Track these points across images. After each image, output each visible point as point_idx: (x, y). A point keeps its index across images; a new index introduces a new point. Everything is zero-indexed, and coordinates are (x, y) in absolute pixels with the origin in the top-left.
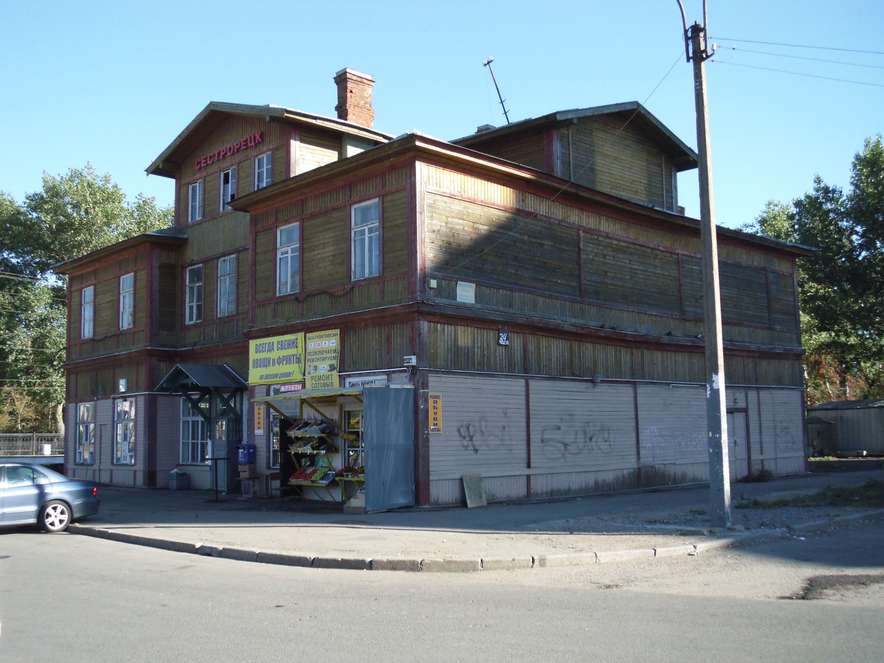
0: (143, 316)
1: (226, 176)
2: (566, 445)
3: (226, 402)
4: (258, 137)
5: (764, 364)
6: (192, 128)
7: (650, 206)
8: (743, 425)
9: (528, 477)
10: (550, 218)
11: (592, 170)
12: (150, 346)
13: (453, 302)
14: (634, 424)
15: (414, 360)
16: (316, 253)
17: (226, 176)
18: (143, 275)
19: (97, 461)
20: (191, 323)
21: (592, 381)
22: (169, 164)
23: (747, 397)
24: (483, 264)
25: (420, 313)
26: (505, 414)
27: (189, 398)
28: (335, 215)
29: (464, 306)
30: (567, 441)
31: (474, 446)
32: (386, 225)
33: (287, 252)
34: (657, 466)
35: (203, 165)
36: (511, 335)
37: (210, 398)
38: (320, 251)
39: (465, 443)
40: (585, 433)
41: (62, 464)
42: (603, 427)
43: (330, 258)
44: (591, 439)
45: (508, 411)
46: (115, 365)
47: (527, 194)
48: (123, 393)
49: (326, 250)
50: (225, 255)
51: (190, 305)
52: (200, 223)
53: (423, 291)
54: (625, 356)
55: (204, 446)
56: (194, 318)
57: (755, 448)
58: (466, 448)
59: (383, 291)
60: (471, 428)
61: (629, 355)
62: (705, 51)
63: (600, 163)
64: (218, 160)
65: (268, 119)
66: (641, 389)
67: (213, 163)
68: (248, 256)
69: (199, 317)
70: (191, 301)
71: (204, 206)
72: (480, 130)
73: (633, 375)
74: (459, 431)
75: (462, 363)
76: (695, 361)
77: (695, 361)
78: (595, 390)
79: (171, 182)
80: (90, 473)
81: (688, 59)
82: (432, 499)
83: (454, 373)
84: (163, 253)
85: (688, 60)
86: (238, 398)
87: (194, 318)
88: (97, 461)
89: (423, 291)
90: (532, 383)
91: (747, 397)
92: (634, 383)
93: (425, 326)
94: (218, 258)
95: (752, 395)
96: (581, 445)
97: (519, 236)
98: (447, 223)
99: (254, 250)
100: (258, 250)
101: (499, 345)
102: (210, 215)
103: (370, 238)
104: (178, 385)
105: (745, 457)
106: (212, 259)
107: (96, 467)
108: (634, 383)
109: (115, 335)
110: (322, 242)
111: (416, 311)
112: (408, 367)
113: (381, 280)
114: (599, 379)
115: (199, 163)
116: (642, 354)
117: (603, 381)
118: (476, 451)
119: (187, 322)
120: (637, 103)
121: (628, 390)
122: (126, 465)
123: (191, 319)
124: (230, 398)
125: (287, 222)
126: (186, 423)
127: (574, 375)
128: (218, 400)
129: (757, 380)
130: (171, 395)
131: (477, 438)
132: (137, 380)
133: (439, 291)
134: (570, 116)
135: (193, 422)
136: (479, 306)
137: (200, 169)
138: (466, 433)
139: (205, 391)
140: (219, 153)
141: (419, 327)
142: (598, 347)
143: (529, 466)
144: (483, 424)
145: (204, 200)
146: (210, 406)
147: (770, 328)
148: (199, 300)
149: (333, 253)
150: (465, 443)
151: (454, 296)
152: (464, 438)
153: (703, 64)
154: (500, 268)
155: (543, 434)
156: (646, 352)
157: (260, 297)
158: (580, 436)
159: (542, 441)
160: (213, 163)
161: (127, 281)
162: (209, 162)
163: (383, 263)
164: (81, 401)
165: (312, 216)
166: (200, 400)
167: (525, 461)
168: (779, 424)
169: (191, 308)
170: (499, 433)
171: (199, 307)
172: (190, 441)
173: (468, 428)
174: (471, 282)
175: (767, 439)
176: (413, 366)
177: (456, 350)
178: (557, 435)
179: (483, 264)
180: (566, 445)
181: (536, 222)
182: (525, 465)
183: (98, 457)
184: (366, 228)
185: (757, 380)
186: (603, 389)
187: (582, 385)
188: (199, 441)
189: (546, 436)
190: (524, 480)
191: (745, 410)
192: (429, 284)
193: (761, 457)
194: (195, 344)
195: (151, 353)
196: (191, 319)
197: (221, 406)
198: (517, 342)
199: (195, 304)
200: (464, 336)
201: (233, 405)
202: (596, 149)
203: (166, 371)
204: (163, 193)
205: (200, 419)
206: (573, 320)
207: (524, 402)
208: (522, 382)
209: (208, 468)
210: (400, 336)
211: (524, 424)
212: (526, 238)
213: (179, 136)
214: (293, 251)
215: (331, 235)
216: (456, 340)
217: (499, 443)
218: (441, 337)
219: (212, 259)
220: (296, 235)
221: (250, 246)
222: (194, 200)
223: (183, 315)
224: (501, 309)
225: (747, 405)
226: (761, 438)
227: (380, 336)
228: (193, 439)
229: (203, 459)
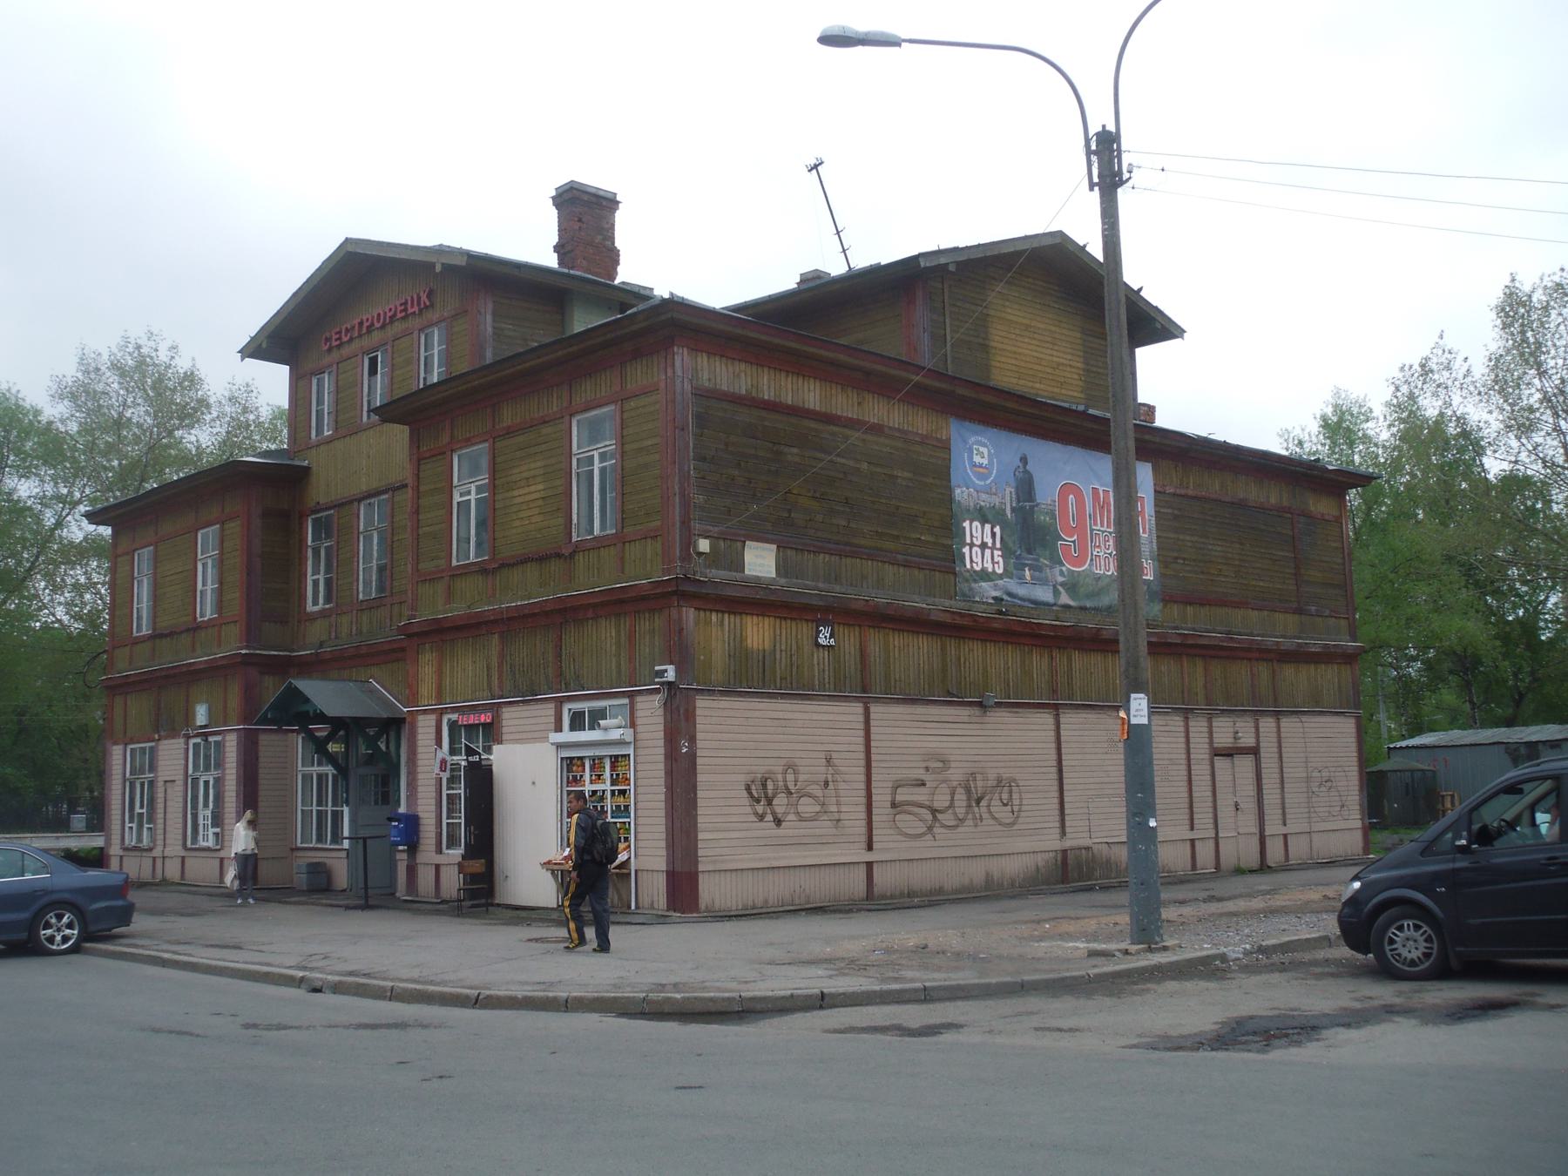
0: (235, 596)
1: (373, 362)
2: (934, 811)
3: (372, 742)
4: (424, 297)
5: (1288, 671)
6: (302, 295)
7: (1081, 408)
8: (1252, 775)
9: (869, 865)
10: (905, 432)
11: (985, 348)
12: (247, 647)
13: (738, 575)
14: (1055, 776)
15: (671, 674)
16: (516, 493)
17: (373, 362)
18: (235, 527)
19: (160, 842)
20: (316, 608)
21: (980, 704)
22: (281, 340)
23: (1279, 727)
24: (789, 511)
25: (685, 597)
26: (829, 760)
27: (310, 735)
28: (546, 430)
29: (758, 584)
30: (936, 805)
31: (774, 814)
32: (628, 447)
33: (469, 493)
34: (1095, 847)
35: (345, 339)
36: (840, 630)
37: (347, 734)
38: (522, 491)
39: (760, 809)
40: (968, 791)
41: (102, 849)
42: (999, 780)
43: (540, 502)
44: (978, 801)
45: (834, 755)
46: (190, 678)
47: (866, 394)
48: (202, 727)
49: (533, 488)
50: (370, 495)
51: (314, 578)
52: (329, 441)
53: (686, 557)
54: (1039, 663)
55: (337, 817)
56: (321, 601)
57: (1272, 815)
58: (761, 818)
59: (622, 559)
60: (770, 785)
61: (1046, 660)
62: (1120, 173)
63: (998, 336)
64: (360, 336)
65: (438, 268)
66: (1068, 718)
67: (351, 339)
68: (406, 497)
69: (328, 599)
70: (316, 571)
71: (337, 413)
72: (804, 279)
73: (1054, 692)
74: (748, 789)
75: (753, 678)
76: (1164, 668)
77: (1164, 668)
78: (987, 719)
79: (284, 370)
80: (147, 863)
81: (1092, 186)
82: (702, 906)
83: (741, 694)
84: (265, 495)
85: (1091, 189)
86: (392, 734)
87: (321, 601)
88: (160, 842)
89: (686, 557)
90: (874, 708)
91: (1279, 727)
92: (1056, 707)
93: (690, 615)
94: (359, 500)
95: (1267, 724)
96: (961, 811)
97: (851, 463)
98: (727, 445)
99: (417, 489)
100: (422, 488)
101: (818, 645)
102: (346, 428)
103: (603, 471)
104: (293, 713)
105: (1255, 830)
106: (351, 502)
107: (157, 852)
108: (1056, 707)
109: (188, 630)
110: (525, 475)
111: (675, 593)
112: (662, 684)
113: (619, 540)
114: (992, 702)
115: (327, 340)
116: (1070, 660)
117: (999, 705)
118: (778, 822)
119: (310, 608)
120: (1061, 232)
121: (1047, 719)
122: (208, 849)
123: (315, 603)
124: (378, 737)
125: (469, 442)
126: (307, 778)
127: (950, 694)
128: (360, 740)
129: (1276, 700)
130: (279, 731)
131: (780, 802)
132: (225, 707)
133: (713, 559)
134: (943, 261)
135: (320, 776)
136: (783, 581)
137: (330, 350)
138: (761, 793)
139: (338, 724)
140: (361, 324)
141: (680, 619)
142: (990, 648)
143: (870, 848)
144: (790, 777)
145: (337, 403)
146: (347, 748)
147: (1299, 611)
148: (328, 569)
149: (543, 494)
150: (760, 809)
151: (740, 567)
152: (758, 801)
153: (1122, 194)
154: (819, 518)
155: (894, 794)
156: (1076, 655)
157: (426, 566)
158: (961, 797)
159: (894, 805)
160: (351, 339)
161: (207, 538)
162: (345, 339)
163: (623, 512)
164: (950, 499)
165: (510, 432)
166: (329, 738)
167: (864, 838)
168: (1316, 774)
169: (316, 583)
170: (819, 793)
171: (328, 582)
172: (315, 808)
173: (764, 786)
174: (767, 541)
175: (1294, 798)
176: (670, 683)
177: (740, 655)
178: (920, 795)
179: (789, 511)
180: (934, 811)
181: (882, 440)
182: (864, 845)
183: (160, 837)
184: (596, 454)
185: (1276, 700)
186: (1002, 717)
187: (963, 713)
188: (330, 808)
189: (899, 798)
190: (861, 872)
191: (1255, 751)
192: (695, 546)
193: (1284, 830)
194: (321, 646)
195: (247, 661)
196: (315, 603)
197: (363, 749)
198: (850, 640)
199: (321, 577)
200: (758, 633)
201: (383, 747)
202: (992, 312)
203: (271, 690)
204: (271, 385)
205: (329, 770)
206: (947, 603)
207: (861, 740)
208: (858, 708)
209: (344, 854)
210: (650, 629)
211: (863, 778)
212: (865, 466)
213: (294, 295)
214: (479, 490)
215: (539, 464)
216: (743, 639)
217: (818, 808)
218: (714, 635)
219: (351, 502)
220: (484, 463)
221: (410, 481)
222: (320, 402)
223: (303, 597)
224: (821, 585)
225: (1258, 742)
226: (1283, 798)
227: (618, 632)
228: (319, 804)
229: (337, 838)
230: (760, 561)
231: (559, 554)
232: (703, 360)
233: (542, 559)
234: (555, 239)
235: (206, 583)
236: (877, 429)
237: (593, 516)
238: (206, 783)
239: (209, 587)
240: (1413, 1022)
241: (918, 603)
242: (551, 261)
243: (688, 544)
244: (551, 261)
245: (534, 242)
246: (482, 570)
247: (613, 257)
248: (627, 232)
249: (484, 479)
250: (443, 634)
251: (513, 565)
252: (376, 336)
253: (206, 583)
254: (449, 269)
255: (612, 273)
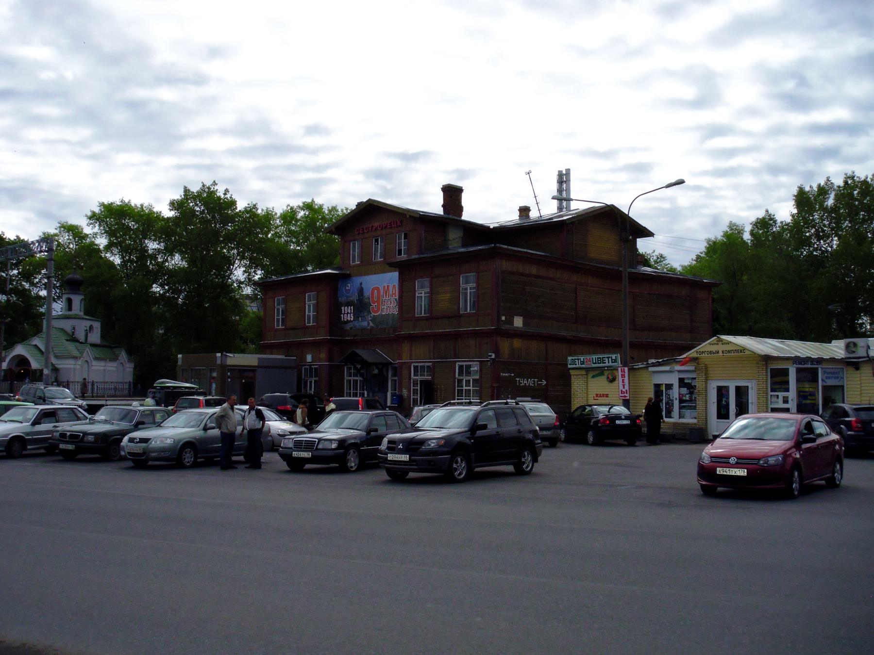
17: (377, 241)
93: (499, 339)
125: (422, 277)
133: (506, 322)
222: (354, 251)
230: (518, 322)
231: (457, 316)
232: (504, 263)
233: (449, 318)
234: (442, 203)
235: (310, 312)
236: (552, 279)
237: (467, 306)
238: (311, 382)
239: (311, 314)
240: (66, 192)
241: (563, 333)
242: (442, 213)
243: (499, 318)
244: (442, 213)
245: (434, 205)
246: (427, 319)
247: (460, 209)
248: (466, 200)
249: (428, 290)
250: (412, 338)
251: (438, 318)
252: (378, 233)
253: (310, 312)
254: (411, 217)
255: (461, 216)
